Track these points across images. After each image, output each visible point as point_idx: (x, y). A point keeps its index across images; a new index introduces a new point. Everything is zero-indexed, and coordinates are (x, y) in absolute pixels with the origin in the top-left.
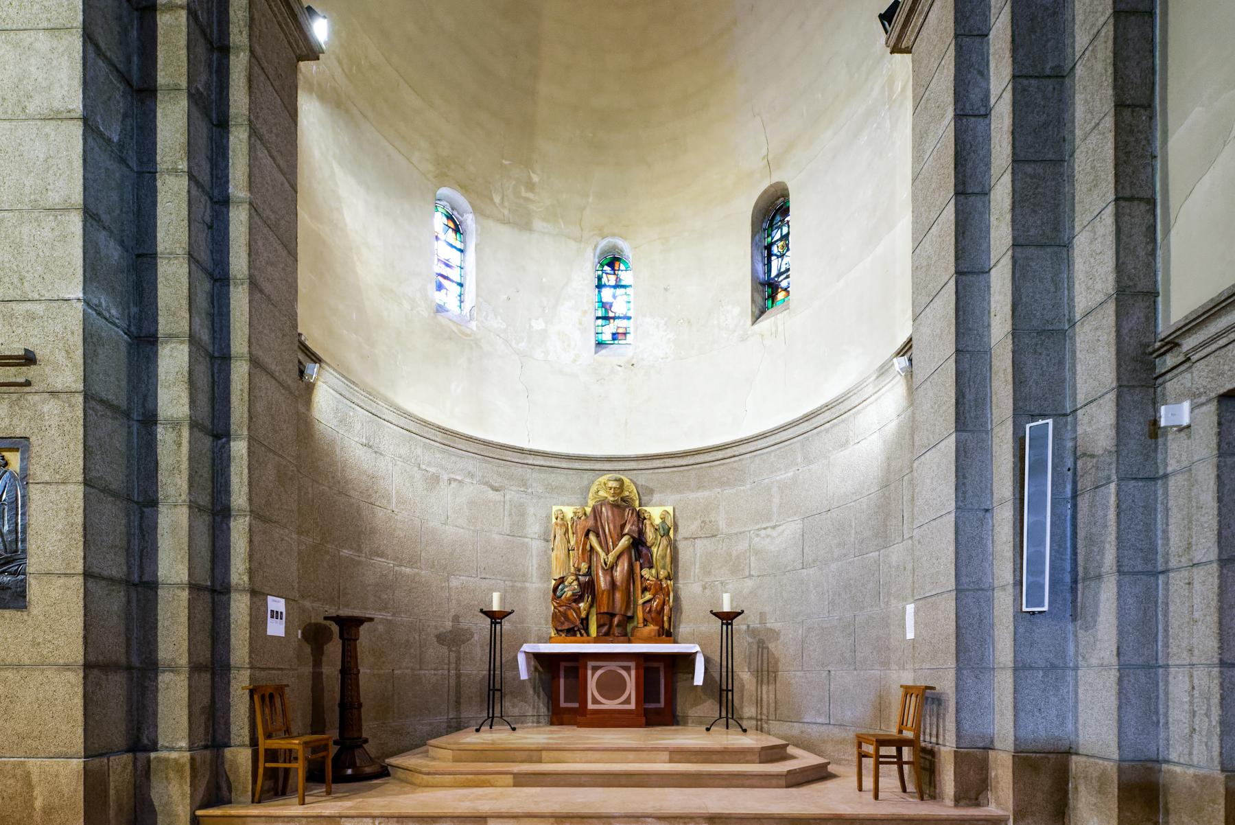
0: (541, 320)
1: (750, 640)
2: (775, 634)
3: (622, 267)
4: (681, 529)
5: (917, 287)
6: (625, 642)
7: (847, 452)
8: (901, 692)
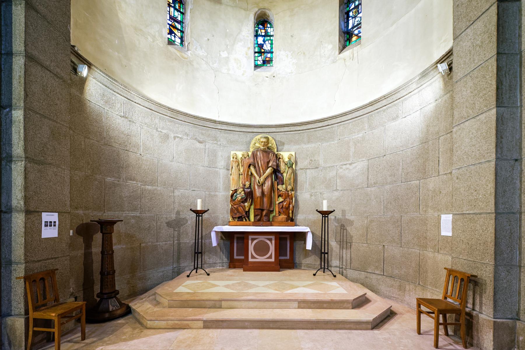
0: (225, 52)
1: (337, 225)
2: (351, 223)
3: (269, 26)
4: (299, 163)
5: (457, 18)
6: (267, 223)
7: (397, 122)
8: (445, 272)
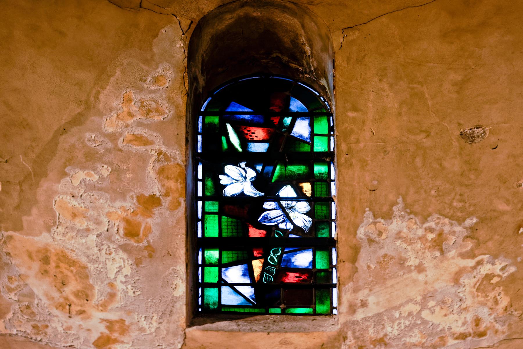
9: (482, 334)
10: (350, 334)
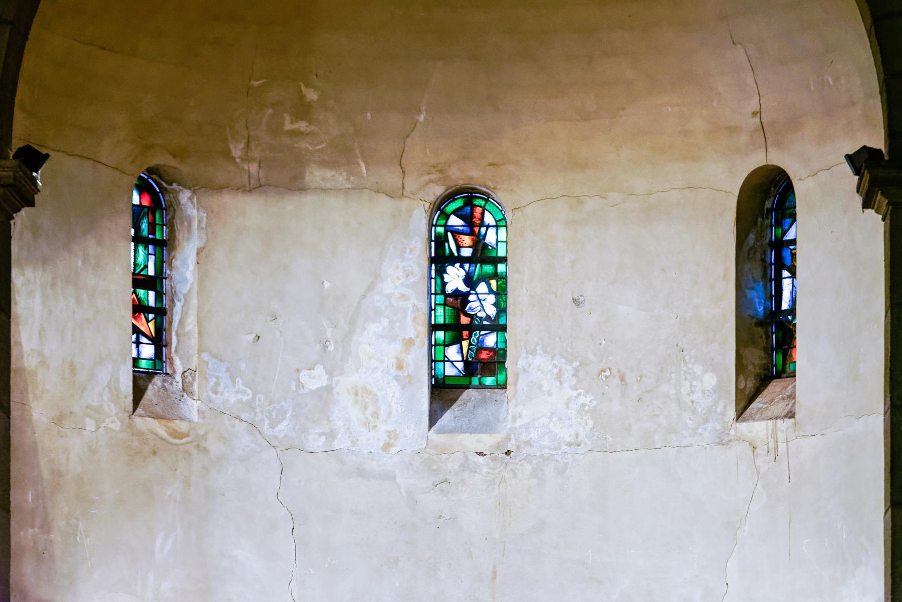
0: (319, 370)
9: (579, 445)
10: (512, 437)
